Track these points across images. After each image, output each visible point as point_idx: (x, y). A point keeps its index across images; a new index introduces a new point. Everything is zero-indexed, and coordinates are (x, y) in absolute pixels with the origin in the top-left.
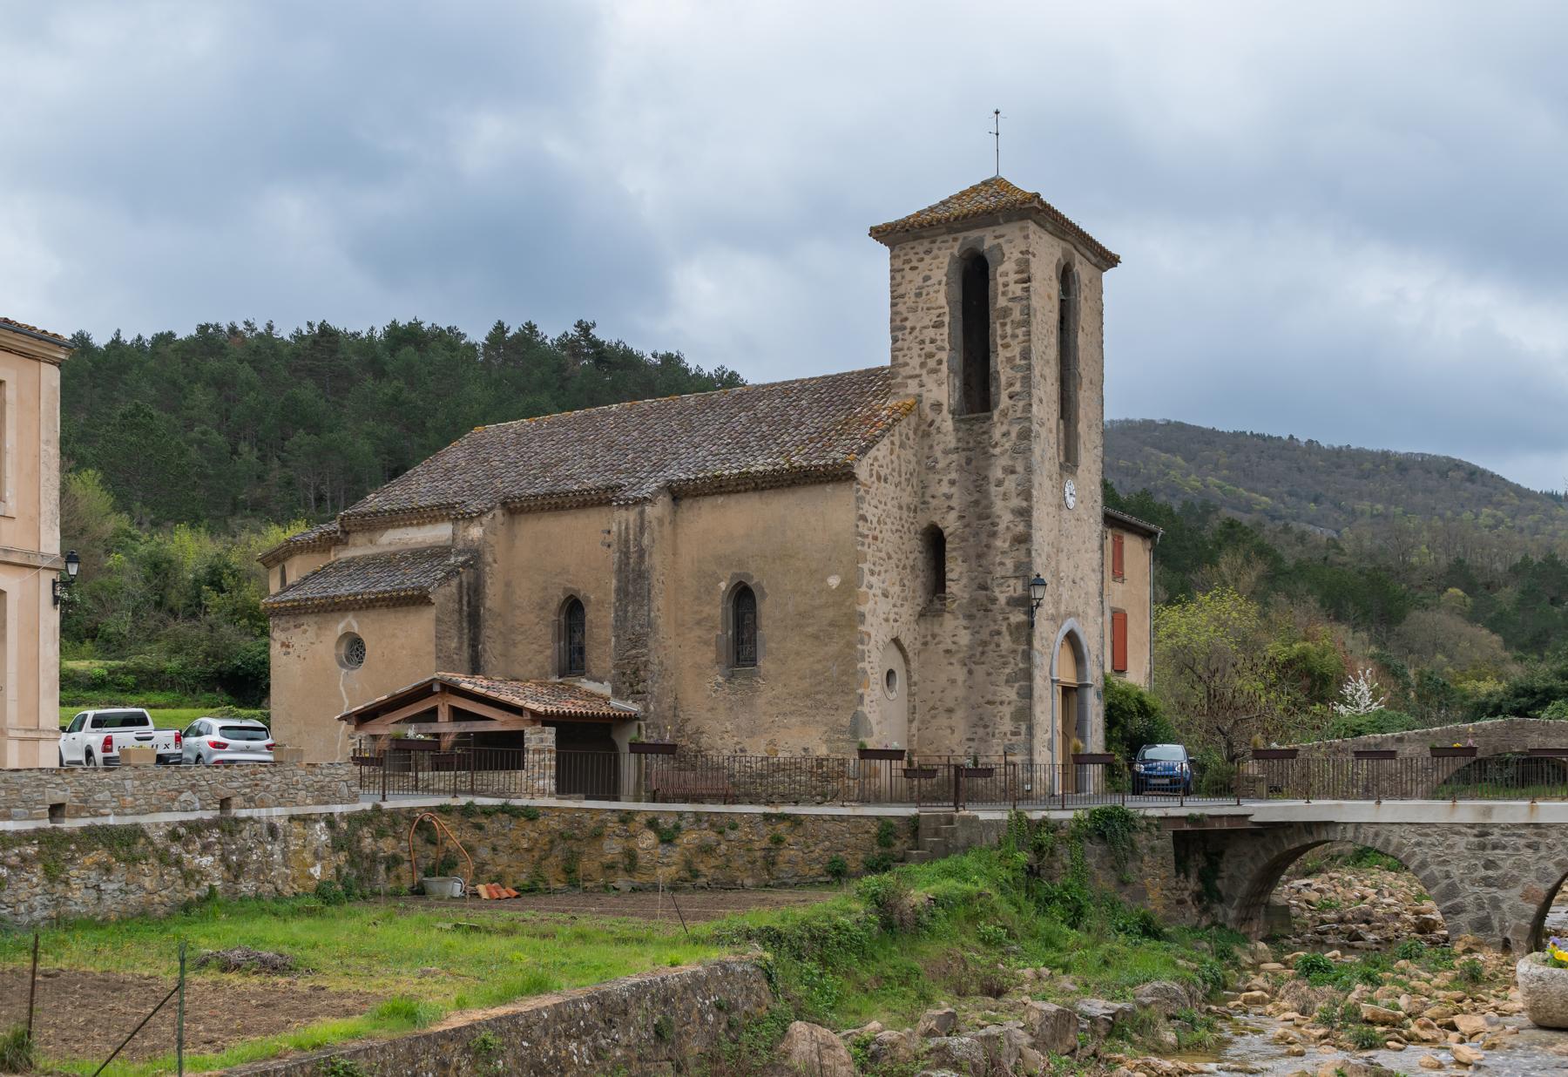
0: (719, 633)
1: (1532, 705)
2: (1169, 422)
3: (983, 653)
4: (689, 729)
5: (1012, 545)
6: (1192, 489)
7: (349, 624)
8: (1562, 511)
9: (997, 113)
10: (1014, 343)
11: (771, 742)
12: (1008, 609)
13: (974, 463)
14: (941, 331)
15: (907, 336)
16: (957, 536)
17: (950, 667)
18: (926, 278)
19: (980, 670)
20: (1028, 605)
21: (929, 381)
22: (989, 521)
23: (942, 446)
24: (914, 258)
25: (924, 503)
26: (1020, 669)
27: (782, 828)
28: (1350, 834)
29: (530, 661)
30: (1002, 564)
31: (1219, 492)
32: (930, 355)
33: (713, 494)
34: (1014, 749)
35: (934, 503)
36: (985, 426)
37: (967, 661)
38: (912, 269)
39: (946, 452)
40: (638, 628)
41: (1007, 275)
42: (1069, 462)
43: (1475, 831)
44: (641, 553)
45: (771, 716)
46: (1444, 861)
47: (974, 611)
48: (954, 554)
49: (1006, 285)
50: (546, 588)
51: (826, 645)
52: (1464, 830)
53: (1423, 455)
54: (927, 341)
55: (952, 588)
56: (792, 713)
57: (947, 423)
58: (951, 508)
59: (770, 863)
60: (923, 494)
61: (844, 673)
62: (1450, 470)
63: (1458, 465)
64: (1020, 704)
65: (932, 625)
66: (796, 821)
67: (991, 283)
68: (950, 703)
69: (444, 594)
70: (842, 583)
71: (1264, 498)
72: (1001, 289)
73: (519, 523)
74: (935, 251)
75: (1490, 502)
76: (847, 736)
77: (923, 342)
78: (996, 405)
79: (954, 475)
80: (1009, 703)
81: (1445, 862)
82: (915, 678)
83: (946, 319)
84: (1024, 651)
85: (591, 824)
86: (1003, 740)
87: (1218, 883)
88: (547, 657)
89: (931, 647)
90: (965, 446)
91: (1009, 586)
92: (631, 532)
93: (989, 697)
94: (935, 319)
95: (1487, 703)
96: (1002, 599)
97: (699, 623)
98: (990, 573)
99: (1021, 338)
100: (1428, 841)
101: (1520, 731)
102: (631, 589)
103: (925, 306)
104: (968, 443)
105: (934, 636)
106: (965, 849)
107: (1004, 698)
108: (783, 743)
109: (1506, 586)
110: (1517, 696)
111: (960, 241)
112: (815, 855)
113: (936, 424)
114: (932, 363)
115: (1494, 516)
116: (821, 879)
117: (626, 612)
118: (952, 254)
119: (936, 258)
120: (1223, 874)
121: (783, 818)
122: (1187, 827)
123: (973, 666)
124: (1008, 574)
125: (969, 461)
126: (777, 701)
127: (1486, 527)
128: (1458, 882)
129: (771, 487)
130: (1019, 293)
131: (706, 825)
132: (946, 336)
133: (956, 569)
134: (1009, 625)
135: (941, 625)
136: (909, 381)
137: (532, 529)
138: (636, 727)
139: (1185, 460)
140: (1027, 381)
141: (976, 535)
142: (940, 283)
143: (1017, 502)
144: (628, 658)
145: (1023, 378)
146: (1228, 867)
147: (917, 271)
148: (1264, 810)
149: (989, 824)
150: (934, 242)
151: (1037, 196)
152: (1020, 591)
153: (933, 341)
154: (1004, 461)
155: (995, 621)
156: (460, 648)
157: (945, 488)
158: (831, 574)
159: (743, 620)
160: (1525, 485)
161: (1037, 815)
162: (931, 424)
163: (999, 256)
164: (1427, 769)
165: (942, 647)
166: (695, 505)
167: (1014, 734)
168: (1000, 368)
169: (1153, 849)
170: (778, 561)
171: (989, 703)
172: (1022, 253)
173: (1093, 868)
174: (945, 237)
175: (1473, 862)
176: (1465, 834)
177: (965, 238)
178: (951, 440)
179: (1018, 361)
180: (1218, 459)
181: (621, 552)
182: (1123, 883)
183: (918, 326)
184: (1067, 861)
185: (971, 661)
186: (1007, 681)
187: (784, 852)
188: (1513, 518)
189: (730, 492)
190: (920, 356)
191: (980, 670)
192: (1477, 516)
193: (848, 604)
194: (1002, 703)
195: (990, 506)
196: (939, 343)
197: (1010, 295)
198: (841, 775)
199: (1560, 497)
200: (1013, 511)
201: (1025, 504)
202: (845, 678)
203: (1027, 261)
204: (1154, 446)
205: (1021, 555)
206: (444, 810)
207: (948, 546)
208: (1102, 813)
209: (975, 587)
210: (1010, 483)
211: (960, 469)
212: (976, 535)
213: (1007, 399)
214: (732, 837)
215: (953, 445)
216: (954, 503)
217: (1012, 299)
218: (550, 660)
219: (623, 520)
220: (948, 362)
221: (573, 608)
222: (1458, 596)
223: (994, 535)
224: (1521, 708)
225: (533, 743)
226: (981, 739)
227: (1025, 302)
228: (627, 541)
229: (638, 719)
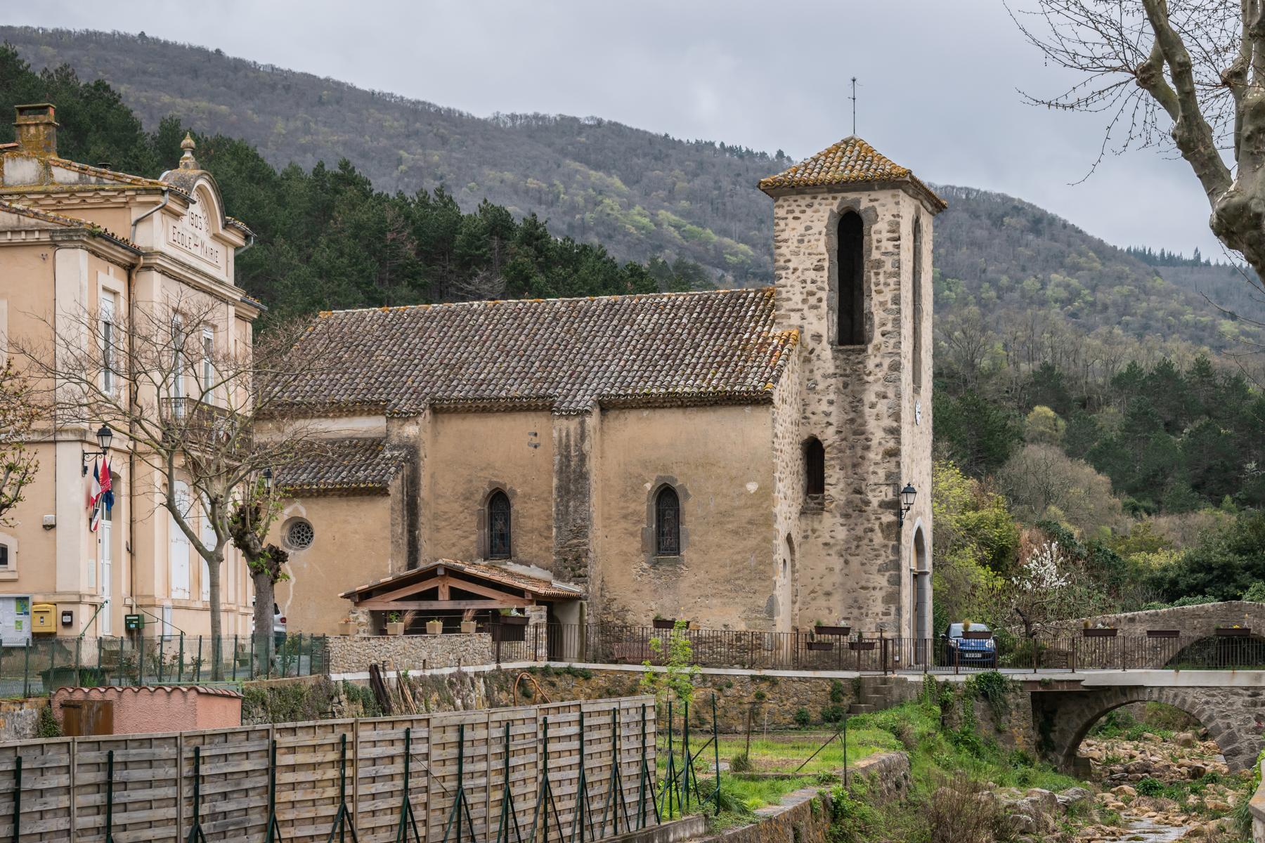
0: (645, 526)
1: (1211, 581)
2: (600, 123)
3: (858, 547)
4: (615, 607)
5: (883, 458)
6: (637, 228)
7: (296, 509)
8: (1159, 281)
9: (854, 80)
10: (886, 290)
12: (880, 511)
13: (850, 387)
14: (820, 273)
15: (790, 276)
16: (835, 447)
17: (828, 558)
18: (808, 228)
19: (855, 561)
20: (895, 506)
21: (811, 315)
22: (863, 437)
23: (821, 371)
24: (797, 210)
25: (805, 418)
27: (764, 686)
28: (1155, 695)
29: (454, 545)
30: (875, 473)
31: (676, 234)
32: (812, 294)
33: (640, 408)
35: (814, 418)
36: (861, 358)
37: (844, 553)
38: (795, 218)
39: (825, 376)
40: (579, 521)
41: (880, 232)
42: (917, 389)
43: (1249, 693)
44: (583, 458)
46: (1226, 716)
47: (850, 511)
48: (832, 462)
49: (879, 241)
50: (471, 481)
51: (745, 539)
52: (1241, 691)
53: (968, 191)
54: (809, 281)
55: (830, 491)
57: (826, 351)
58: (829, 424)
59: (754, 714)
60: (804, 410)
61: (761, 563)
62: (1006, 214)
63: (1018, 208)
65: (812, 521)
66: (773, 681)
67: (866, 238)
68: (828, 588)
69: (395, 486)
70: (760, 488)
71: (743, 247)
72: (875, 244)
73: (443, 422)
74: (816, 206)
75: (1062, 265)
76: (764, 615)
77: (804, 281)
78: (870, 341)
79: (832, 397)
80: (881, 589)
81: (1227, 716)
82: (798, 566)
83: (826, 264)
84: (893, 546)
85: (628, 683)
87: (1052, 735)
88: (472, 542)
89: (811, 540)
90: (842, 372)
92: (572, 439)
93: (863, 583)
94: (816, 263)
95: (1162, 579)
96: (875, 502)
97: (625, 517)
98: (864, 480)
99: (892, 287)
100: (1214, 700)
101: (1237, 613)
102: (572, 487)
103: (807, 252)
104: (845, 370)
105: (814, 531)
106: (901, 703)
107: (876, 584)
108: (705, 620)
109: (1108, 404)
110: (1193, 571)
111: (839, 200)
112: (787, 708)
113: (816, 352)
114: (813, 300)
115: (1067, 286)
116: (792, 726)
117: (567, 507)
118: (832, 211)
119: (817, 211)
120: (1056, 728)
121: (764, 679)
122: (1040, 689)
123: (849, 558)
125: (846, 385)
127: (1056, 301)
128: (1236, 731)
129: (695, 406)
130: (891, 249)
131: (710, 684)
132: (825, 279)
133: (835, 479)
134: (881, 524)
135: (820, 522)
136: (792, 314)
137: (456, 428)
138: (578, 606)
139: (625, 181)
140: (897, 322)
141: (852, 447)
142: (820, 233)
143: (889, 423)
144: (570, 546)
145: (894, 320)
146: (1060, 723)
147: (799, 221)
148: (1091, 676)
149: (914, 685)
150: (815, 198)
151: (910, 172)
153: (813, 282)
154: (878, 388)
155: (868, 520)
156: (402, 534)
157: (824, 407)
158: (749, 480)
159: (664, 516)
160: (1110, 242)
161: (941, 679)
162: (811, 352)
163: (873, 216)
164: (1156, 647)
165: (821, 540)
166: (621, 416)
167: (886, 614)
168: (873, 309)
169: (1018, 705)
171: (863, 588)
172: (893, 216)
173: (978, 720)
174: (826, 195)
175: (1248, 716)
176: (1242, 695)
177: (843, 198)
178: (830, 367)
179: (889, 306)
180: (674, 184)
181: (562, 455)
182: (999, 731)
184: (962, 714)
185: (847, 553)
186: (879, 571)
187: (765, 705)
188: (1094, 289)
190: (802, 293)
191: (855, 561)
192: (1044, 285)
193: (765, 506)
194: (874, 588)
195: (864, 424)
196: (819, 284)
197: (883, 250)
198: (759, 647)
199: (1155, 257)
200: (884, 430)
201: (895, 424)
202: (762, 567)
203: (898, 224)
204: (577, 158)
205: (892, 466)
206: (531, 670)
207: (827, 456)
208: (986, 677)
209: (851, 491)
210: (882, 406)
211: (838, 391)
212: (852, 447)
213: (880, 336)
214: (729, 693)
215: (832, 370)
216: (832, 419)
217: (885, 254)
218: (475, 545)
219: (564, 428)
220: (828, 300)
221: (498, 501)
222: (1048, 418)
223: (867, 448)
224: (1198, 584)
226: (856, 619)
227: (896, 257)
228: (568, 446)
229: (580, 599)
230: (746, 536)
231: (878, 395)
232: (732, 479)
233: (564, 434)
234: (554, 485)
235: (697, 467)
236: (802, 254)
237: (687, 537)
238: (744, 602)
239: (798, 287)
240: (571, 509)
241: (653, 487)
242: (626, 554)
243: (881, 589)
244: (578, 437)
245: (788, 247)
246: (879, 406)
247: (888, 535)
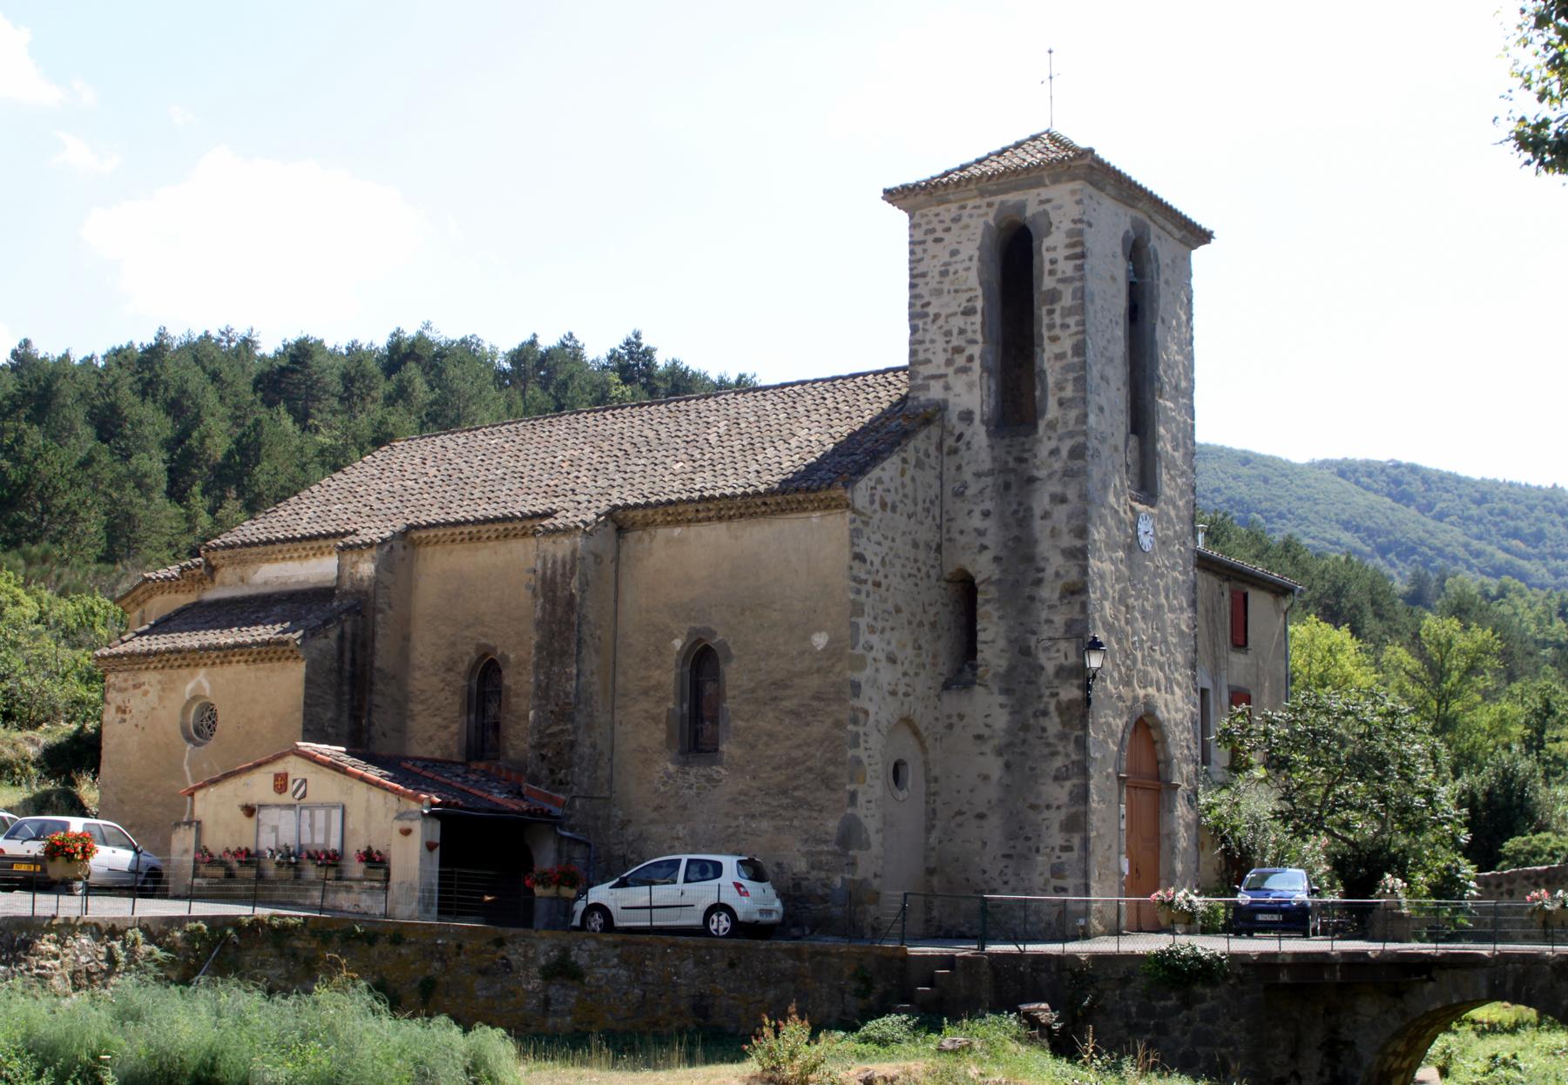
5: (1062, 597)
9: (1050, 52)
12: (1056, 683)
18: (954, 253)
21: (959, 383)
26: (1073, 763)
32: (958, 350)
56: (762, 815)
70: (830, 642)
72: (1047, 267)
86: (1049, 856)
91: (1058, 651)
97: (645, 692)
114: (960, 361)
136: (932, 382)
167: (1067, 848)
193: (837, 669)
197: (1059, 275)
230: (809, 718)
243: (1058, 807)
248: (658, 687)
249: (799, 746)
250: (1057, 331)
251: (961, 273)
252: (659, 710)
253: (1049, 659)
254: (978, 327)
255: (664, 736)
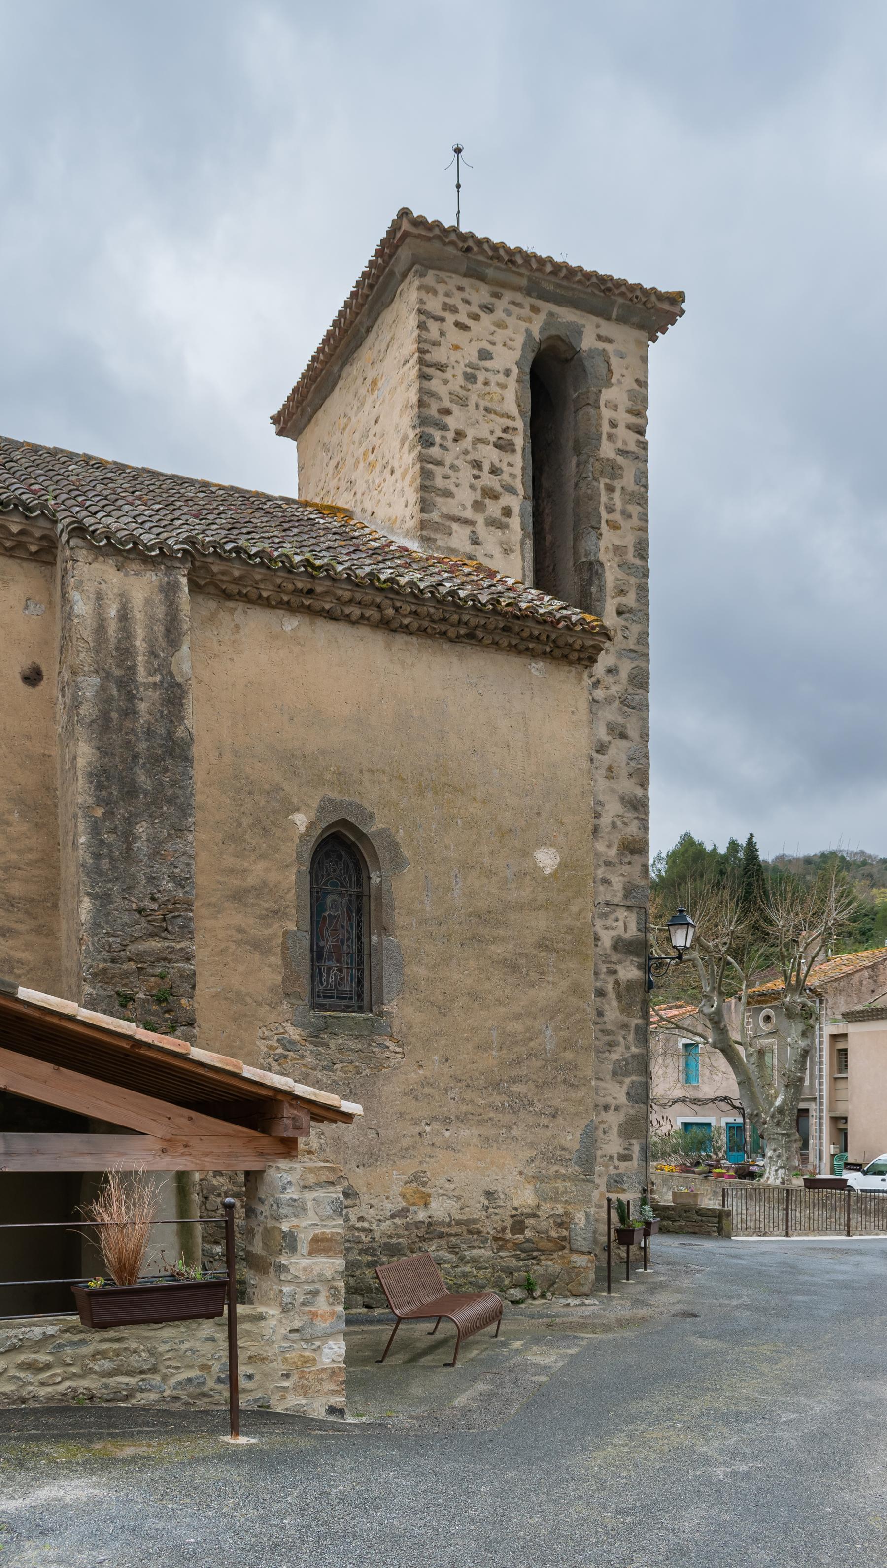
5: (620, 854)
9: (458, 151)
10: (626, 525)
11: (415, 1178)
12: (615, 957)
14: (508, 458)
15: (449, 443)
18: (484, 355)
21: (490, 539)
26: (633, 1056)
30: (606, 881)
32: (490, 494)
34: (622, 1182)
45: (416, 1122)
54: (486, 467)
56: (462, 1119)
64: (632, 1112)
70: (563, 866)
72: (606, 428)
74: (499, 314)
76: (574, 1169)
86: (606, 1166)
91: (617, 920)
97: (238, 896)
102: (143, 779)
103: (483, 404)
107: (609, 1100)
108: (441, 1180)
114: (494, 509)
117: (128, 837)
118: (528, 332)
119: (501, 325)
124: (617, 900)
126: (427, 1090)
129: (422, 632)
134: (617, 982)
136: (455, 526)
142: (507, 373)
144: (139, 957)
147: (467, 335)
152: (633, 931)
153: (494, 471)
158: (541, 843)
163: (604, 371)
167: (625, 1158)
170: (429, 794)
174: (519, 297)
177: (551, 314)
181: (107, 676)
183: (471, 433)
186: (614, 1074)
189: (330, 616)
190: (472, 487)
193: (575, 909)
197: (620, 445)
198: (563, 1244)
200: (622, 799)
202: (569, 1055)
217: (622, 453)
225: (311, 1218)
228: (125, 652)
230: (533, 976)
231: (611, 728)
232: (504, 834)
233: (113, 612)
234: (81, 763)
235: (421, 792)
236: (472, 407)
237: (399, 967)
238: (530, 1138)
239: (466, 473)
240: (141, 845)
241: (311, 826)
242: (240, 997)
243: (617, 1109)
244: (159, 629)
245: (446, 382)
246: (612, 751)
247: (630, 1005)
248: (261, 890)
249: (518, 1017)
250: (617, 517)
251: (493, 388)
252: (267, 932)
253: (606, 928)
254: (518, 471)
255: (279, 978)
